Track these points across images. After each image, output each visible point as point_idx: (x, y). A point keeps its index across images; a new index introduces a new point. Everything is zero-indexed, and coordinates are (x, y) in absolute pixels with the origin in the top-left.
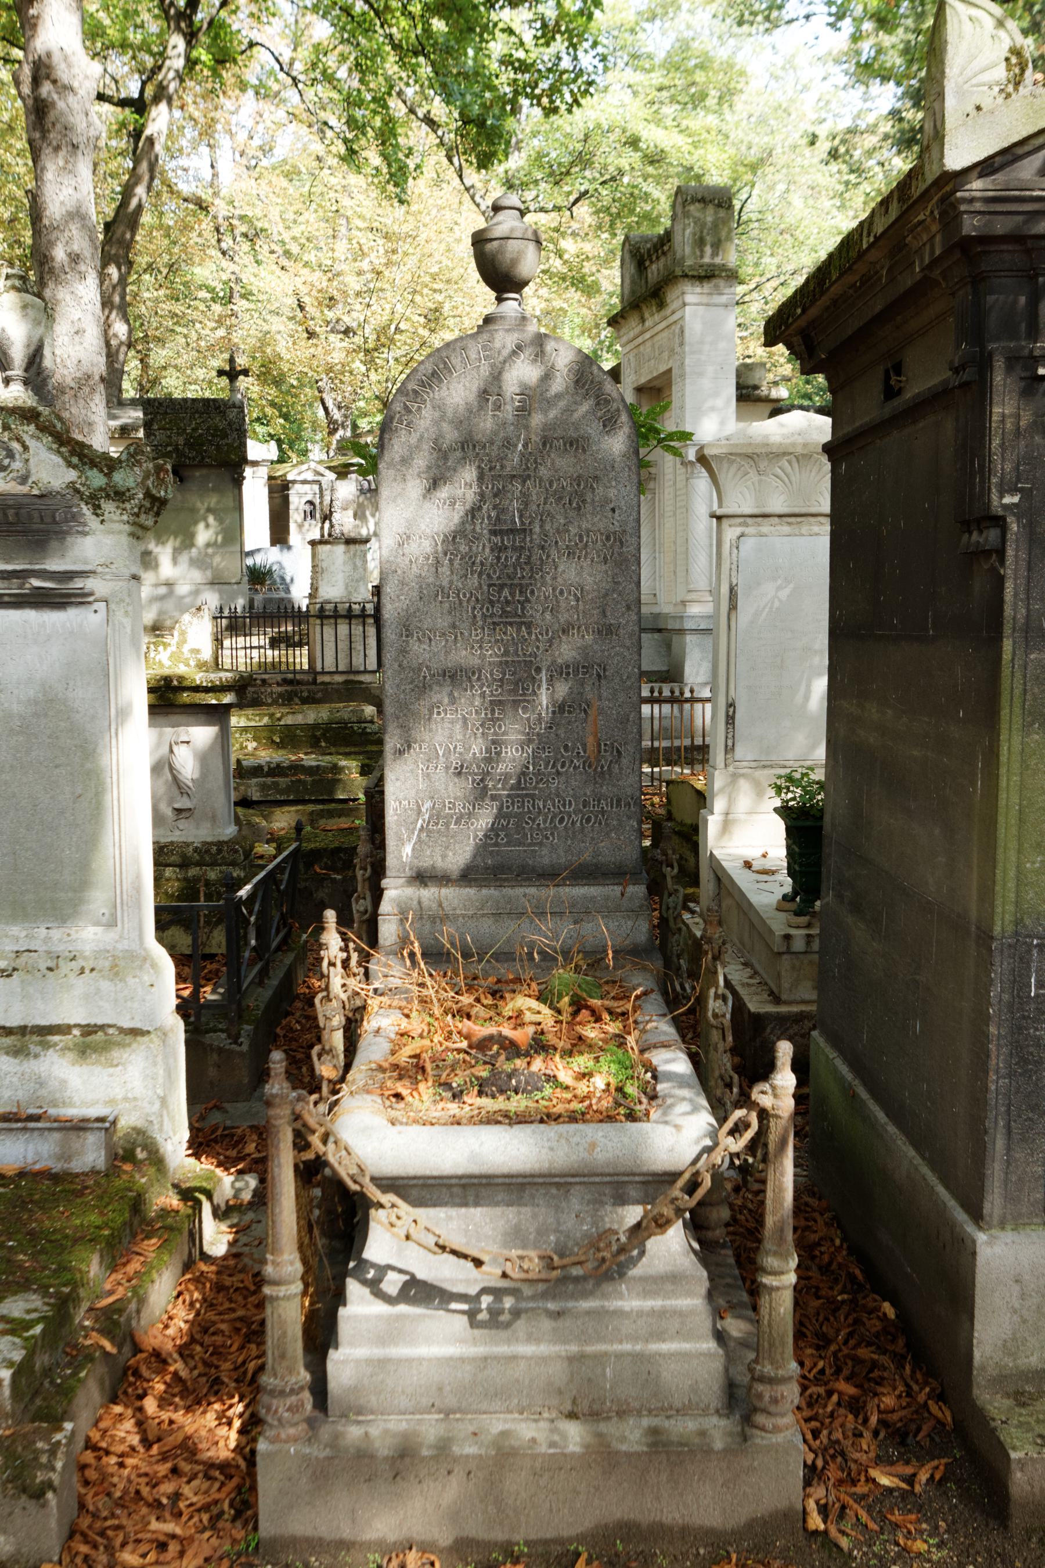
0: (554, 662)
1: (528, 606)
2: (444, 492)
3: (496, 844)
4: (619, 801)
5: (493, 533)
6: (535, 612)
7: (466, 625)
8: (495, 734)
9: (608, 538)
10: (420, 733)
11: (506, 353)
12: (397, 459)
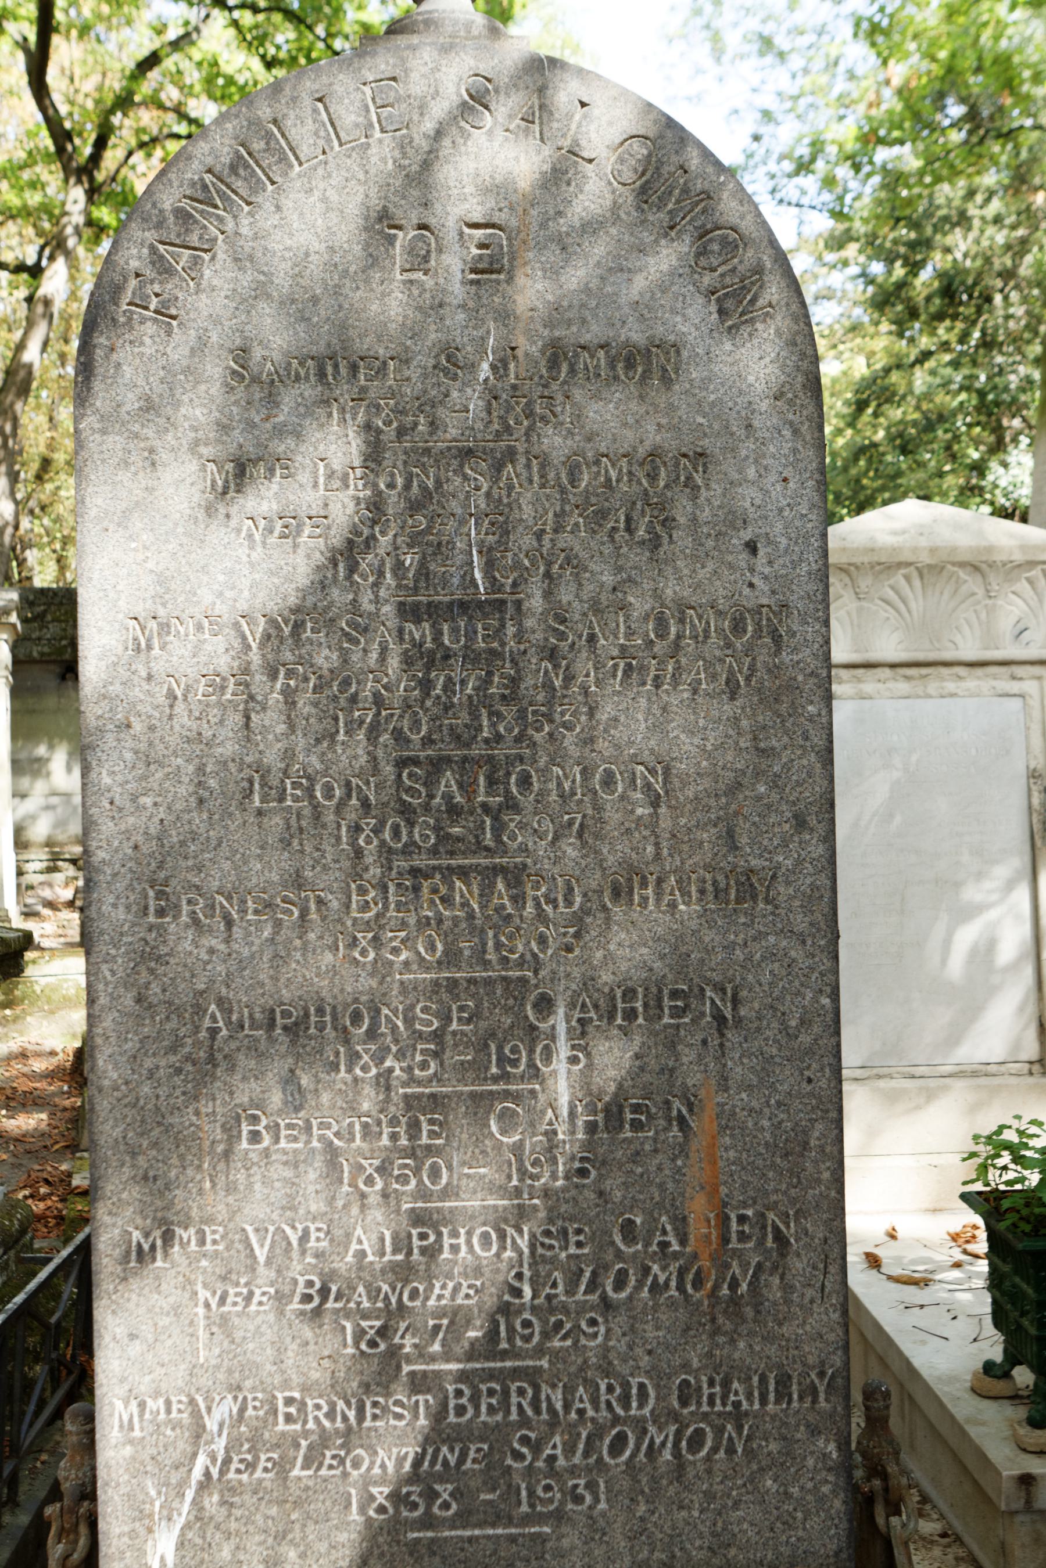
0: (588, 982)
1: (513, 822)
2: (264, 498)
3: (428, 1522)
4: (784, 1382)
5: (409, 612)
6: (530, 839)
7: (334, 876)
8: (422, 1193)
9: (738, 627)
10: (205, 1198)
11: (439, 110)
12: (131, 402)
